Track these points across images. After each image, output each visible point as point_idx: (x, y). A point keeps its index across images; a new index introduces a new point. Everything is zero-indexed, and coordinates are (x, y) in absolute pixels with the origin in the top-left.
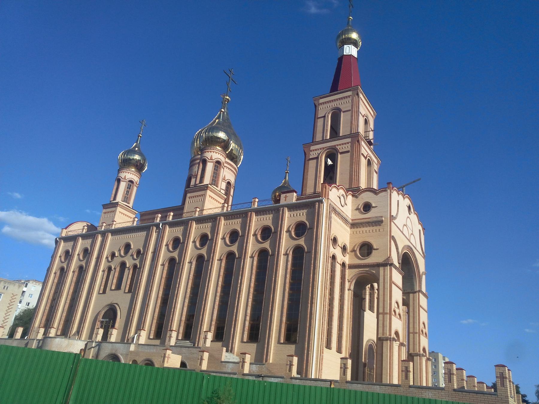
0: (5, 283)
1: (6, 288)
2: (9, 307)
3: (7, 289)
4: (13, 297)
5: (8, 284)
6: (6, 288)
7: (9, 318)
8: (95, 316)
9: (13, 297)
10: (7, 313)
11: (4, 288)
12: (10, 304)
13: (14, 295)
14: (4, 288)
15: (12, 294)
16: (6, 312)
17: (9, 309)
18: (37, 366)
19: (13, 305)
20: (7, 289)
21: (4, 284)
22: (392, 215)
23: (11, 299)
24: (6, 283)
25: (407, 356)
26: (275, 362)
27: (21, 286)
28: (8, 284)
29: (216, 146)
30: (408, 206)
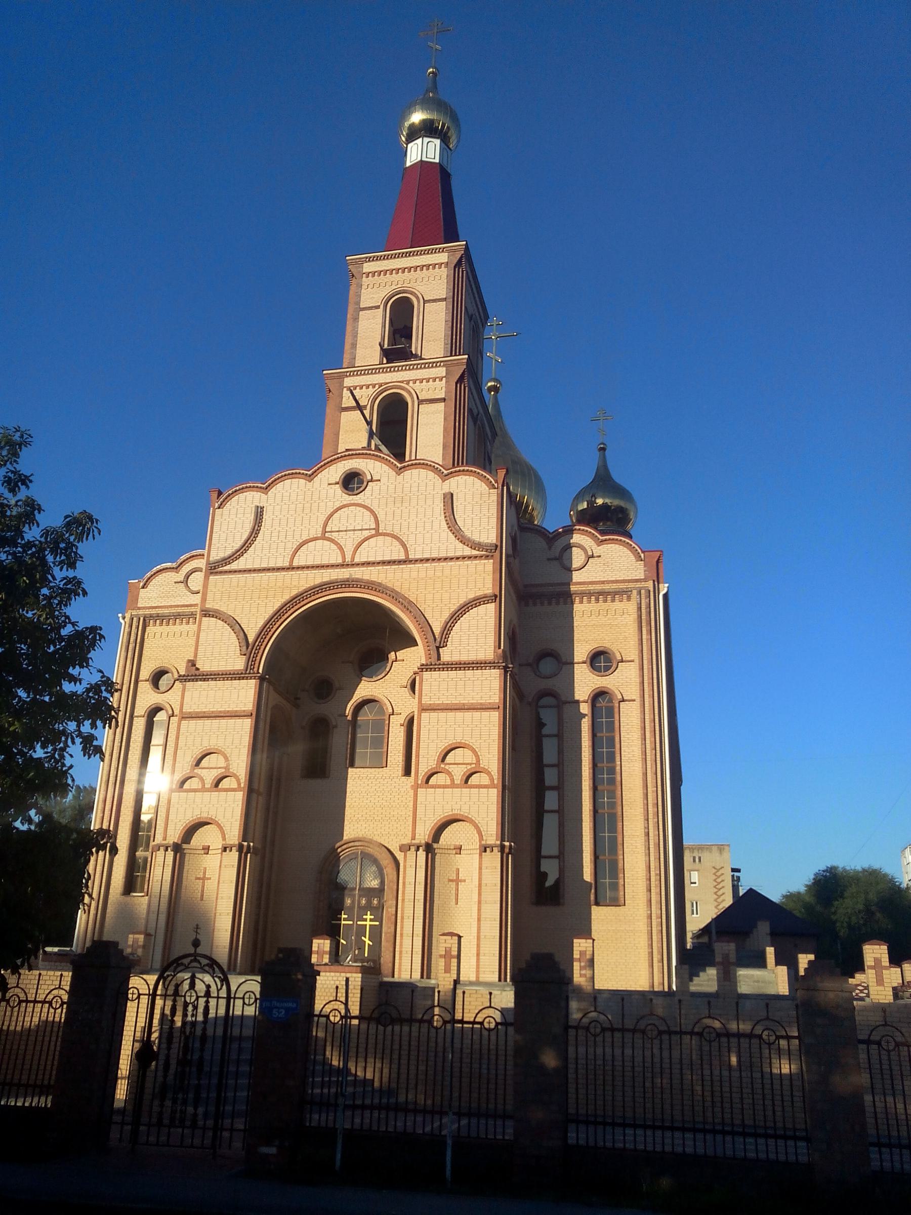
0: (693, 852)
1: (697, 860)
2: (718, 893)
3: (700, 860)
4: (717, 874)
5: (698, 850)
6: (697, 860)
7: (723, 874)
8: (133, 806)
9: (717, 874)
10: (719, 905)
11: (694, 861)
12: (717, 887)
13: (718, 868)
14: (694, 861)
15: (714, 868)
16: (716, 904)
17: (719, 896)
18: (197, 932)
19: (723, 887)
20: (700, 860)
21: (691, 854)
22: (542, 869)
23: (716, 884)
24: (695, 851)
25: (510, 819)
26: (870, 1121)
27: (724, 849)
28: (698, 850)
29: (35, 831)
30: (42, 512)
